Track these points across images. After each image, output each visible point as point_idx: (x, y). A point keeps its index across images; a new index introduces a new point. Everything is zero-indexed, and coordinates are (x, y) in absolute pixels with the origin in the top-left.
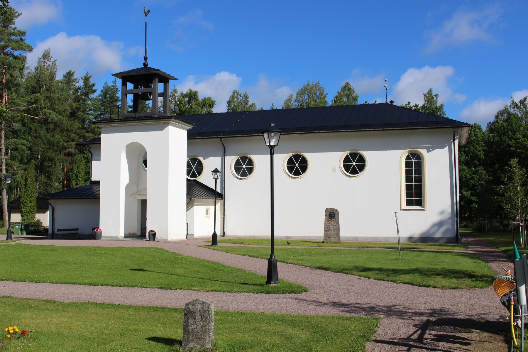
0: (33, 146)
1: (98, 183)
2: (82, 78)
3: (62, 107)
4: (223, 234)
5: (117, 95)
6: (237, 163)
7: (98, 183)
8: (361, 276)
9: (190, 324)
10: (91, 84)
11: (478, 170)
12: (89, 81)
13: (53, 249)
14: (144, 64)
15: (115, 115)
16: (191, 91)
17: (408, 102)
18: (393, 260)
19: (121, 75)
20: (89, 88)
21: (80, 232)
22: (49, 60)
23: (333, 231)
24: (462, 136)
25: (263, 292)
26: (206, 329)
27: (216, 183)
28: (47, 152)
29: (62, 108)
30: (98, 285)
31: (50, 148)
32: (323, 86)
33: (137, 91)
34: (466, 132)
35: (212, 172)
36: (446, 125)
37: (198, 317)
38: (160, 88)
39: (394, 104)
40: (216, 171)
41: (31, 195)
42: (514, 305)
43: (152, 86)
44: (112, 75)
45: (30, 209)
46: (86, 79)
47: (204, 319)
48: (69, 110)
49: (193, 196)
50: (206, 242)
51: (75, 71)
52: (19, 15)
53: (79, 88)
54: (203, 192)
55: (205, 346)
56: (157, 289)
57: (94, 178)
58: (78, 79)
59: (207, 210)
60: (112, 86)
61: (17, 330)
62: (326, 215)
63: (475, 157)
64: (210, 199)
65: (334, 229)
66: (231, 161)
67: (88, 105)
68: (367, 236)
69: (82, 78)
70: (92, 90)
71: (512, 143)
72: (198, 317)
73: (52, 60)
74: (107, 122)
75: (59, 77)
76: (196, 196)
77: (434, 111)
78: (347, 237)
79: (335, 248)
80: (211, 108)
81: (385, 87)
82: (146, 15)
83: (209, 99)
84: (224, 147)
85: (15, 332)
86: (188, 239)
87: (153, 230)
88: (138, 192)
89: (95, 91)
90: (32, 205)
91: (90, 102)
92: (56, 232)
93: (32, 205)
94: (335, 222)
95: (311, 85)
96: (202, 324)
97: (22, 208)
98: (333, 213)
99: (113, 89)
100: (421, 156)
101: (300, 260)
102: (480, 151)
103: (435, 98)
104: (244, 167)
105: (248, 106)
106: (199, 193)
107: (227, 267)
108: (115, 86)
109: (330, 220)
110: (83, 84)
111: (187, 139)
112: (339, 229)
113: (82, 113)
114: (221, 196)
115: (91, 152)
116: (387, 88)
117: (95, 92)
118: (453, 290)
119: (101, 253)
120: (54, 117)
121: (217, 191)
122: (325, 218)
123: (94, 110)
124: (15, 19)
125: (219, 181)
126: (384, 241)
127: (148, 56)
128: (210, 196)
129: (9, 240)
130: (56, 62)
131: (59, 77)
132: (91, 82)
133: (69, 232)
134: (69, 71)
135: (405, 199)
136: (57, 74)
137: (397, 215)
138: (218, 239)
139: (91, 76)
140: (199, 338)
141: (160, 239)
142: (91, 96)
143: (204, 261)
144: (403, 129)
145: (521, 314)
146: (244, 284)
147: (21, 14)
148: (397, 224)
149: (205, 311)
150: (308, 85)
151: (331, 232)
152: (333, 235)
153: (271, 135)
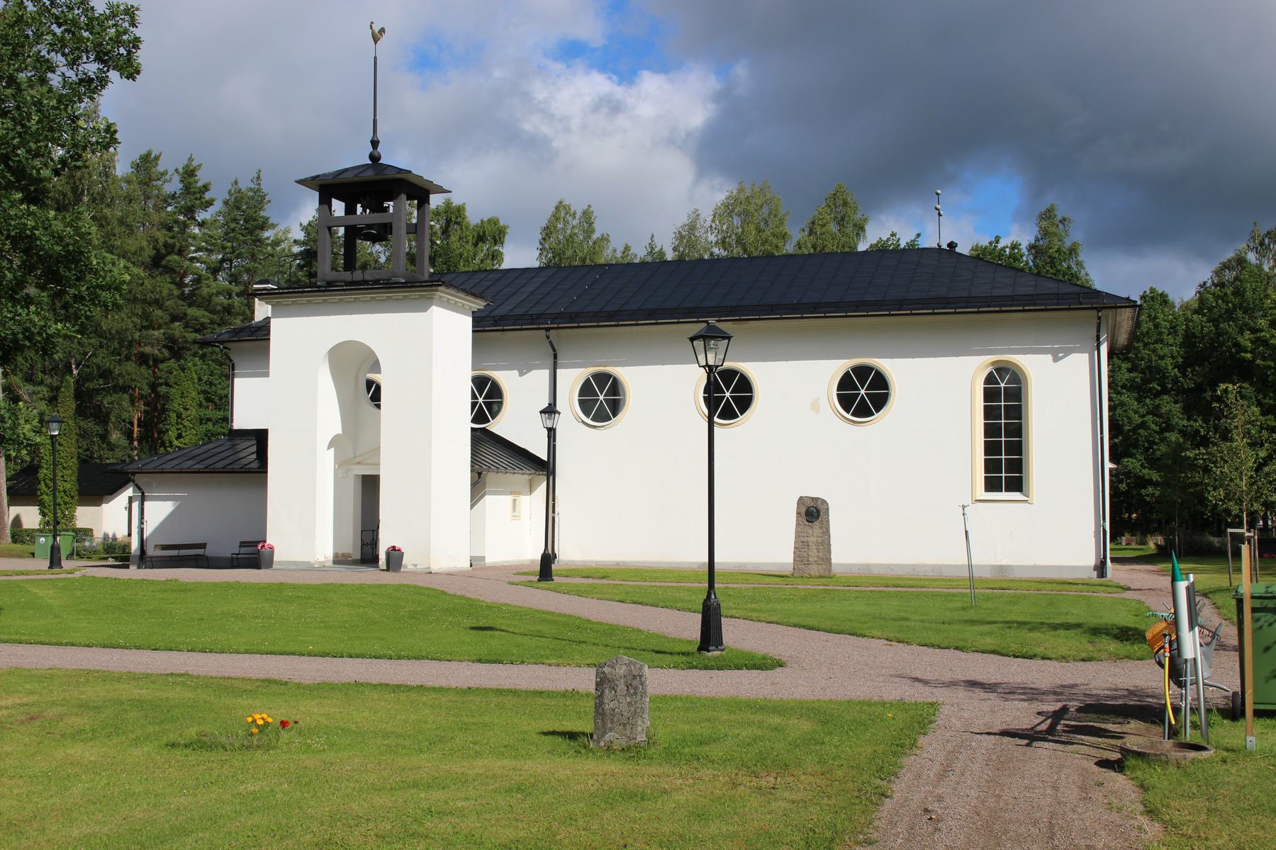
1: (260, 437)
2: (176, 170)
5: (262, 213)
6: (586, 389)
7: (260, 437)
9: (606, 701)
10: (200, 184)
11: (1159, 405)
13: (184, 588)
14: (372, 157)
15: (260, 264)
17: (996, 237)
18: (957, 609)
19: (318, 182)
21: (210, 551)
24: (1119, 328)
25: (695, 667)
26: (638, 708)
28: (94, 355)
29: (132, 244)
31: (101, 347)
33: (352, 220)
34: (1126, 318)
35: (541, 412)
36: (1081, 303)
37: (621, 687)
38: (411, 211)
39: (957, 250)
41: (66, 463)
42: (1170, 658)
44: (297, 182)
45: (62, 497)
46: (189, 173)
47: (632, 691)
48: (149, 252)
49: (484, 467)
50: (519, 574)
53: (173, 196)
54: (505, 460)
55: (636, 738)
57: (243, 419)
61: (270, 720)
62: (798, 513)
63: (1154, 372)
65: (817, 544)
66: (571, 379)
67: (194, 237)
68: (894, 562)
71: (1246, 339)
72: (621, 687)
74: (291, 293)
77: (1055, 258)
79: (823, 587)
80: (495, 244)
81: (937, 209)
82: (376, 40)
83: (493, 222)
84: (554, 350)
85: (267, 724)
87: (398, 545)
88: (355, 457)
89: (210, 203)
90: (69, 486)
91: (196, 231)
93: (68, 486)
94: (821, 528)
96: (628, 699)
97: (42, 494)
98: (816, 508)
99: (253, 198)
100: (1021, 377)
101: (754, 610)
102: (1168, 354)
104: (601, 397)
108: (259, 190)
109: (807, 523)
111: (473, 331)
113: (176, 257)
114: (545, 468)
115: (231, 361)
116: (941, 212)
117: (212, 204)
118: (1082, 663)
123: (207, 250)
126: (931, 574)
127: (380, 136)
129: (56, 570)
132: (199, 180)
133: (183, 552)
134: (146, 153)
135: (983, 475)
137: (966, 512)
139: (200, 166)
140: (624, 725)
142: (201, 216)
143: (537, 611)
144: (978, 312)
145: (1186, 676)
146: (658, 652)
148: (966, 532)
149: (634, 677)
151: (810, 553)
152: (816, 559)
153: (709, 345)
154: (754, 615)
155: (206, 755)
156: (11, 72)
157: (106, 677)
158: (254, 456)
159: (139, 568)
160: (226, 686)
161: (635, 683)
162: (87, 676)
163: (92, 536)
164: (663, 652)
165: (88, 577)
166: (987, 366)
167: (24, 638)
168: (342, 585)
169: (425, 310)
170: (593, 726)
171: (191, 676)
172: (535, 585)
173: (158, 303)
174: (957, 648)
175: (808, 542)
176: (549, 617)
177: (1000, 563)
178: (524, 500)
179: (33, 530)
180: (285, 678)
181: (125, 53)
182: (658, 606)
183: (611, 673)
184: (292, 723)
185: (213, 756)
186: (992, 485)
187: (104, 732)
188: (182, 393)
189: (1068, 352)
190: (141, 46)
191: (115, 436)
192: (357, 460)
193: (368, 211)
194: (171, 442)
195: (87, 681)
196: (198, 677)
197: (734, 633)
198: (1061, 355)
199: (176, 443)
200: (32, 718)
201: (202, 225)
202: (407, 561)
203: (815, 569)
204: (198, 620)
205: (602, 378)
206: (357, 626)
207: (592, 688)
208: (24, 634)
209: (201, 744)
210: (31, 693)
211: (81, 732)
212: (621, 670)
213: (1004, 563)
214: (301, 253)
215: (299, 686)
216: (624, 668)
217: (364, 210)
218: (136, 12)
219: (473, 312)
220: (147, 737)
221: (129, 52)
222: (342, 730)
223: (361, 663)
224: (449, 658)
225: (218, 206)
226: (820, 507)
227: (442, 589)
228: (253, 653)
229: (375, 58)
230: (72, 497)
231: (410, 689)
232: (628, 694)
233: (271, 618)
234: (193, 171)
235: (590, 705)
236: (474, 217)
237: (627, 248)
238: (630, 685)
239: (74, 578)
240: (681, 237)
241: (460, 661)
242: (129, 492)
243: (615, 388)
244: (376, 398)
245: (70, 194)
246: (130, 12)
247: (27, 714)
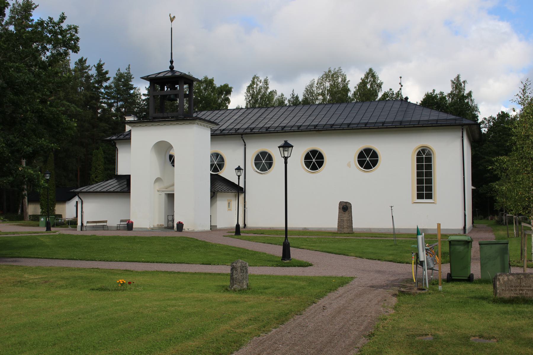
1: (128, 178)
4: (243, 226)
5: (130, 83)
6: (257, 159)
7: (128, 178)
8: (357, 257)
10: (104, 71)
12: (102, 69)
17: (433, 90)
20: (102, 75)
23: (346, 223)
25: (279, 266)
27: (239, 179)
30: (154, 262)
32: (345, 72)
35: (236, 169)
37: (239, 270)
40: (239, 169)
43: (177, 87)
44: (140, 78)
46: (99, 67)
49: (216, 190)
51: (87, 58)
52: (36, 7)
54: (225, 187)
56: (200, 265)
58: (90, 66)
59: (229, 203)
60: (126, 73)
61: (125, 282)
64: (232, 192)
67: (102, 93)
68: (380, 227)
69: (94, 66)
72: (239, 270)
76: (219, 190)
78: (362, 229)
83: (226, 86)
85: (124, 283)
86: (212, 229)
87: (181, 221)
89: (108, 79)
91: (103, 91)
92: (85, 224)
95: (333, 72)
96: (241, 274)
97: (41, 201)
101: (311, 246)
103: (463, 85)
105: (268, 93)
106: (221, 187)
107: (251, 251)
108: (129, 73)
109: (343, 212)
110: (96, 72)
119: (141, 241)
120: (73, 109)
121: (240, 185)
122: (339, 211)
124: (33, 11)
125: (242, 178)
128: (232, 190)
129: (48, 232)
132: (104, 69)
133: (98, 224)
136: (71, 63)
137: (392, 209)
138: (241, 230)
139: (104, 63)
140: (240, 282)
141: (187, 230)
142: (105, 84)
143: (230, 247)
147: (38, 6)
148: (392, 216)
150: (330, 71)
154: (311, 248)
155: (103, 292)
156: (33, 52)
157: (70, 269)
158: (126, 186)
160: (111, 272)
161: (244, 269)
162: (63, 269)
163: (62, 217)
164: (270, 261)
165: (62, 234)
167: (39, 256)
168: (158, 237)
170: (230, 283)
171: (100, 269)
172: (233, 237)
174: (379, 260)
175: (343, 219)
176: (233, 249)
177: (423, 228)
179: (38, 215)
180: (132, 269)
181: (73, 43)
182: (277, 245)
183: (236, 266)
184: (132, 283)
185: (105, 292)
186: (420, 196)
187: (70, 286)
190: (79, 41)
193: (169, 89)
195: (63, 271)
196: (102, 269)
197: (295, 254)
200: (46, 282)
202: (185, 227)
203: (346, 230)
204: (103, 250)
206: (161, 252)
207: (230, 272)
208: (39, 255)
209: (101, 289)
210: (44, 274)
211: (62, 286)
212: (239, 265)
213: (424, 228)
214: (145, 100)
215: (137, 272)
216: (240, 264)
217: (168, 89)
218: (77, 28)
220: (84, 288)
221: (75, 43)
222: (149, 285)
223: (160, 265)
224: (192, 263)
225: (112, 80)
227: (197, 238)
228: (122, 261)
229: (172, 28)
231: (175, 273)
233: (130, 249)
234: (102, 65)
235: (229, 277)
236: (218, 84)
237: (282, 95)
238: (242, 269)
239: (56, 235)
240: (307, 90)
241: (196, 264)
242: (76, 199)
244: (173, 163)
246: (76, 29)
247: (44, 280)
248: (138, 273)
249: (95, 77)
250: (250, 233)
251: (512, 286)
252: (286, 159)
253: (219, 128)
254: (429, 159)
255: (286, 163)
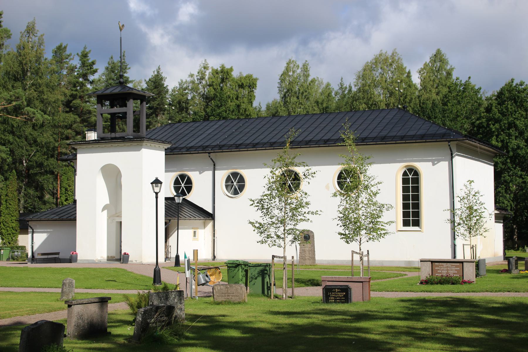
0: (16, 148)
3: (52, 96)
5: (125, 75)
6: (228, 179)
10: (90, 61)
12: (88, 58)
16: (223, 67)
21: (61, 256)
22: (35, 34)
28: (34, 155)
37: (67, 286)
65: (309, 251)
66: (222, 175)
69: (78, 54)
70: (92, 70)
72: (67, 286)
73: (39, 34)
75: (48, 55)
78: (341, 261)
82: (121, 30)
83: (249, 77)
84: (214, 162)
89: (95, 71)
90: (14, 225)
93: (14, 225)
97: (2, 229)
110: (80, 62)
112: (314, 251)
120: (39, 117)
130: (43, 37)
131: (48, 55)
132: (90, 59)
133: (50, 256)
134: (60, 44)
139: (90, 51)
141: (135, 262)
142: (91, 78)
150: (381, 55)
159: (32, 263)
166: (403, 168)
169: (139, 151)
173: (70, 127)
178: (201, 232)
188: (68, 178)
189: (439, 161)
191: (47, 197)
192: (117, 215)
194: (62, 203)
198: (436, 162)
199: (65, 203)
201: (92, 83)
203: (308, 262)
205: (235, 175)
212: (68, 281)
213: (410, 260)
219: (165, 149)
226: (311, 235)
229: (121, 38)
230: (16, 231)
232: (69, 287)
234: (86, 54)
243: (242, 180)
245: (20, 72)
248: (16, 293)
249: (79, 68)
250: (201, 265)
251: (223, 293)
252: (157, 194)
253: (188, 144)
254: (416, 180)
255: (157, 198)
